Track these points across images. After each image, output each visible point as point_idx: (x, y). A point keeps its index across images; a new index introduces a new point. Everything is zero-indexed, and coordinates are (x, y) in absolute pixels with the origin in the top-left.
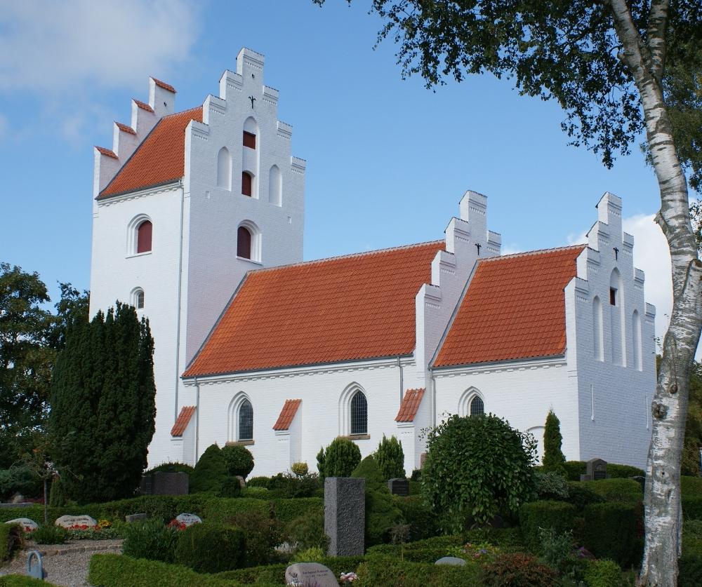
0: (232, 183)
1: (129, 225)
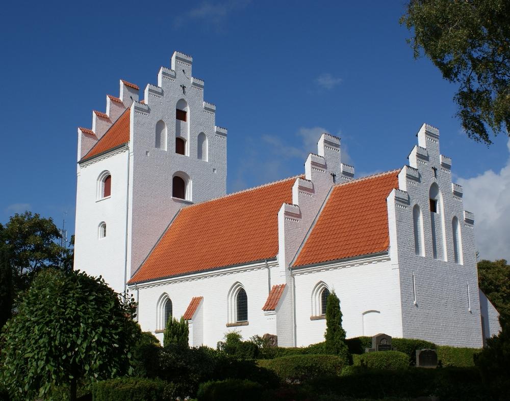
0: (168, 143)
1: (98, 180)
